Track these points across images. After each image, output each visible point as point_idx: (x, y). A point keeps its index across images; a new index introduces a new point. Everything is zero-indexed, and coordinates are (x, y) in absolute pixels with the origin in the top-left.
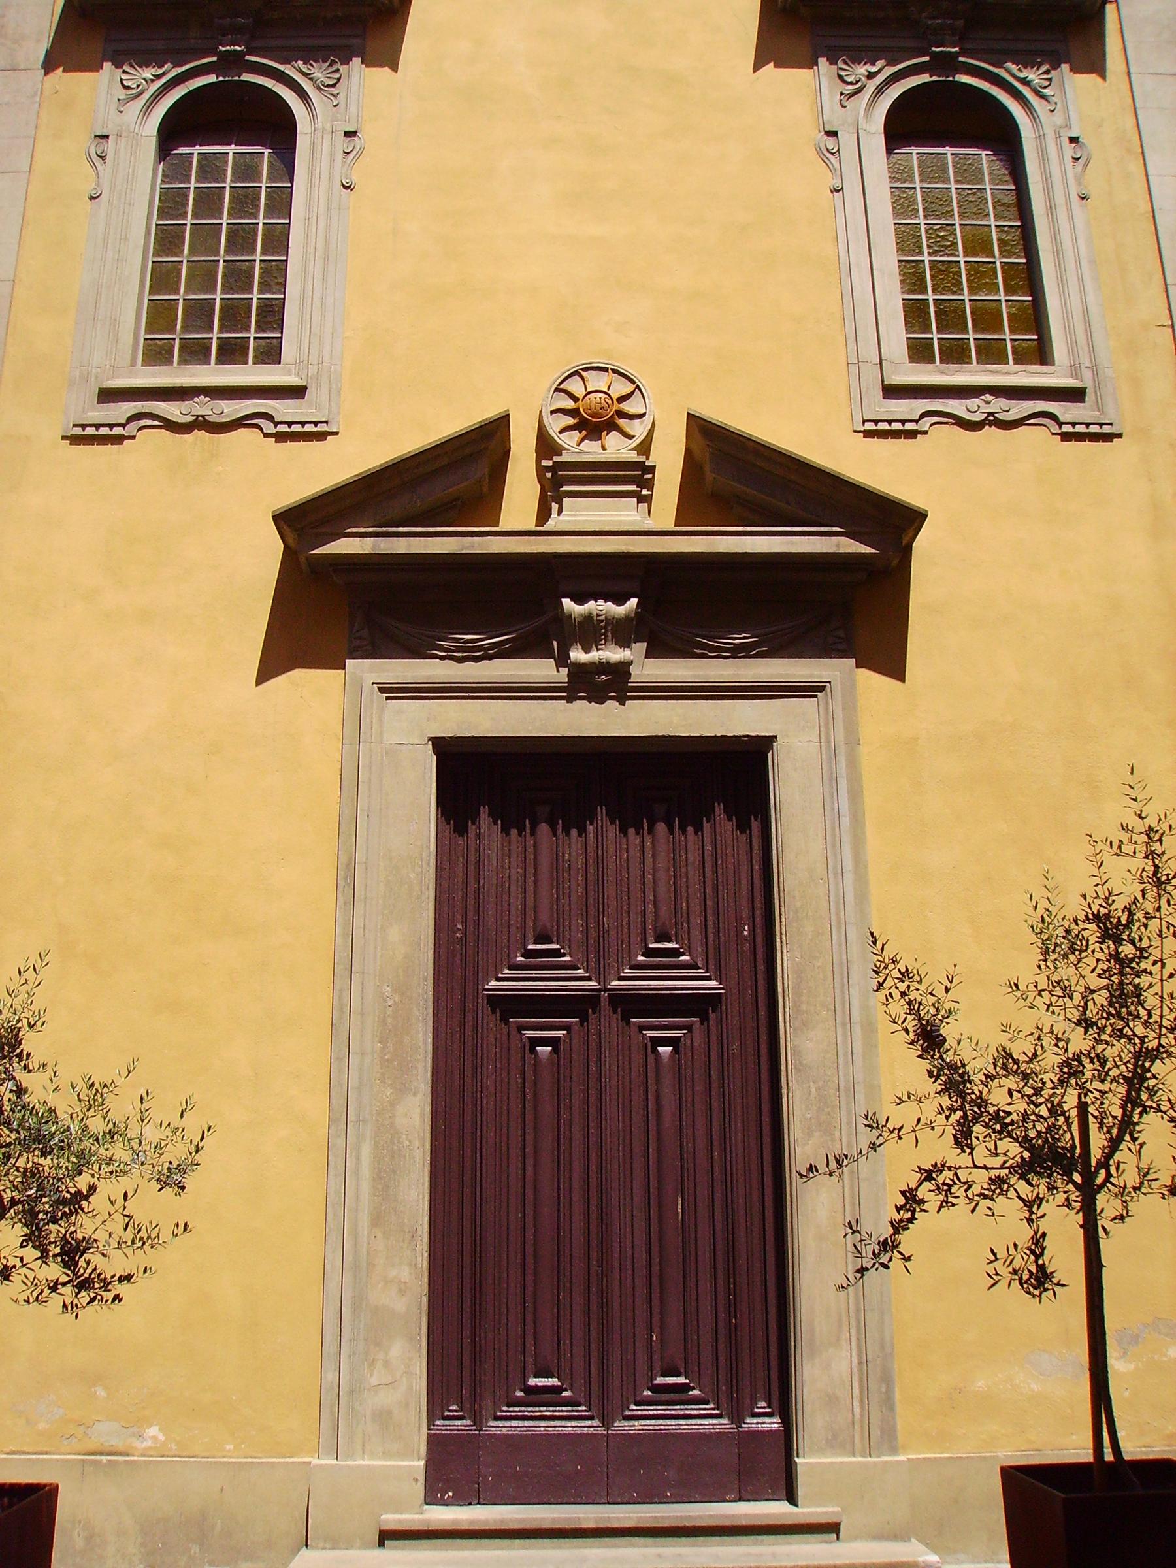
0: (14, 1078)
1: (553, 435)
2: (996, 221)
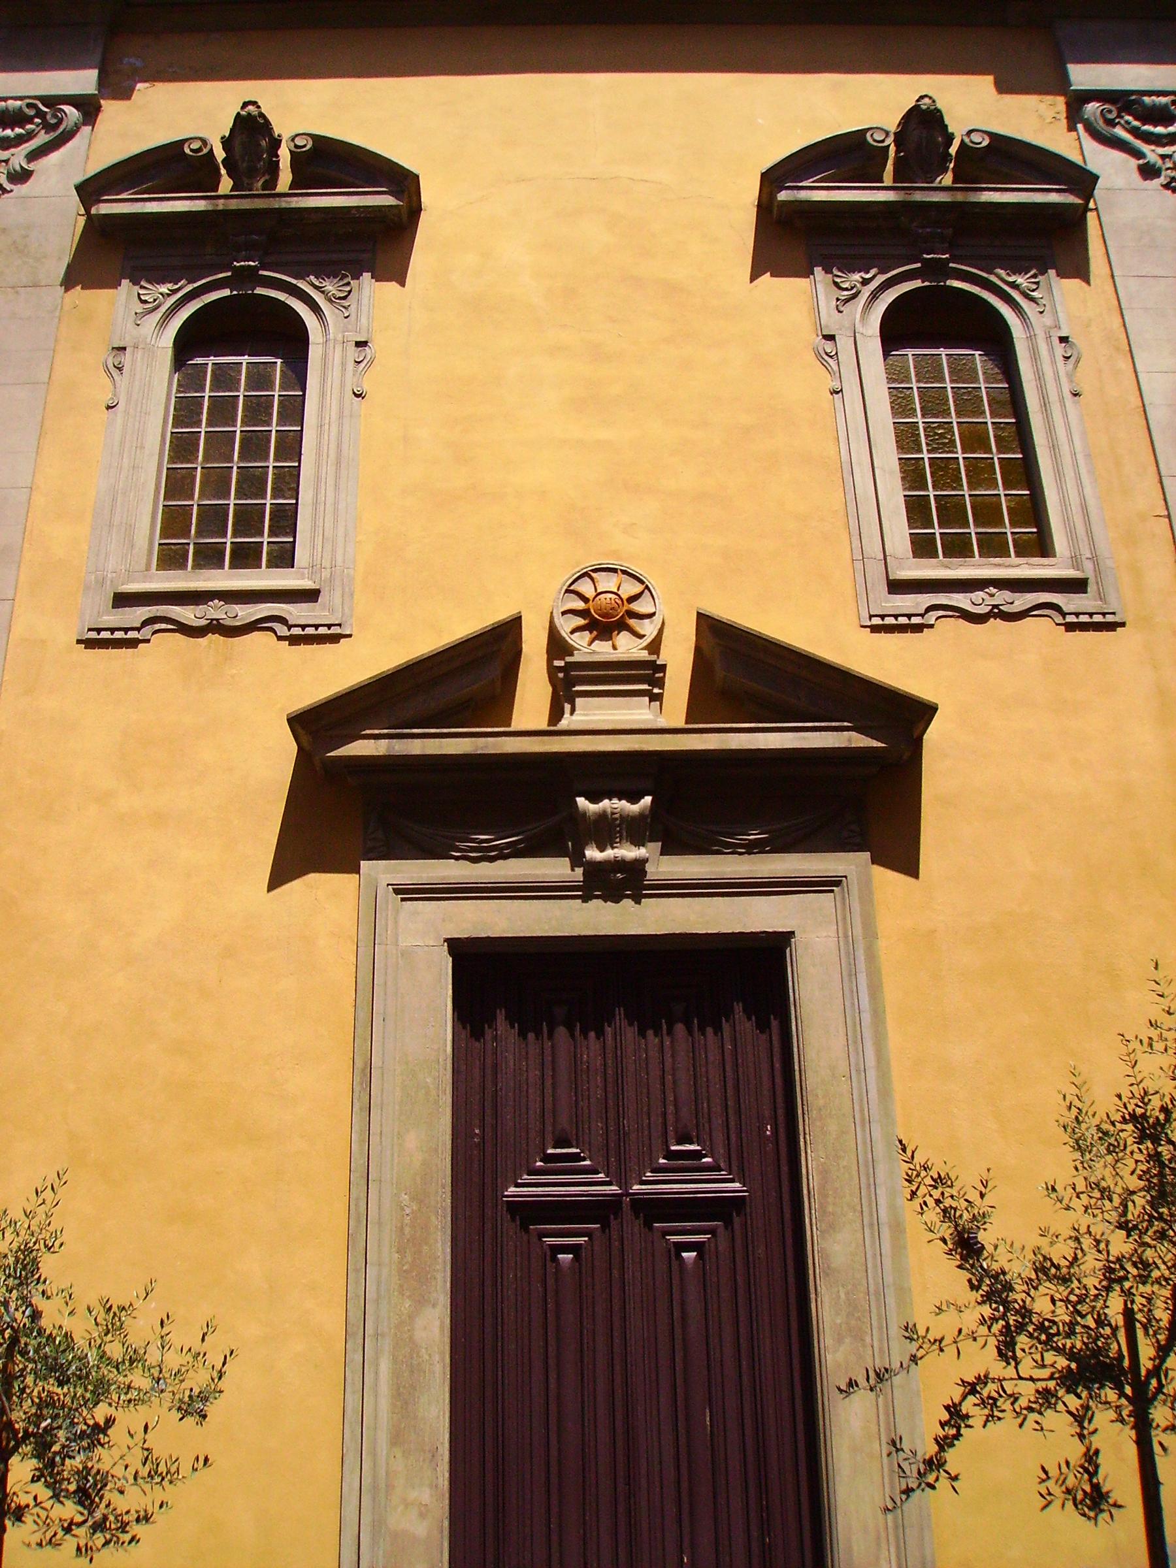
0: (31, 1305)
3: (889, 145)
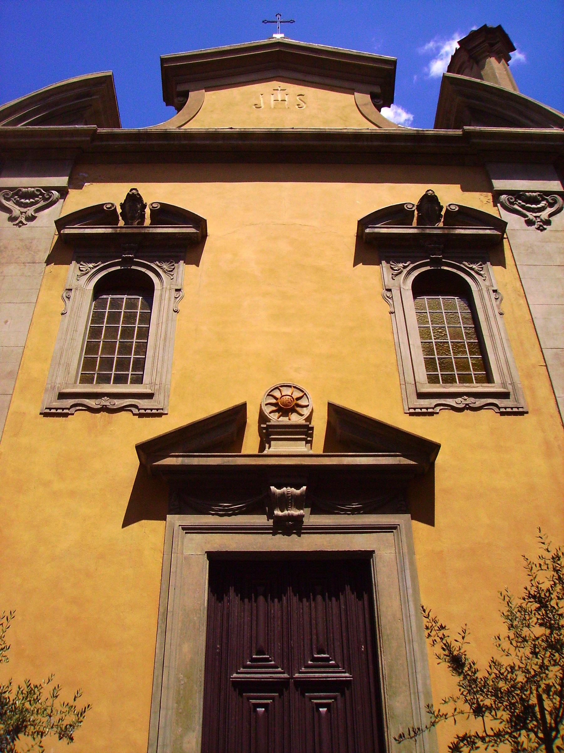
1: (266, 414)
3: (415, 210)
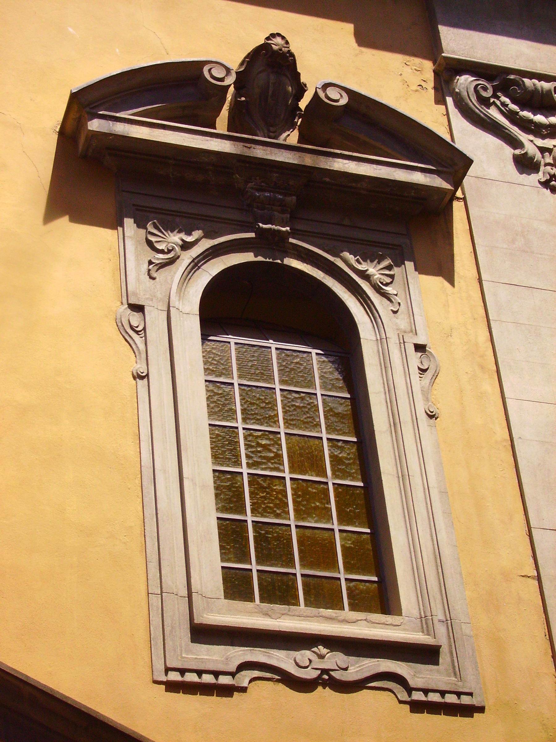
2: (287, 427)
